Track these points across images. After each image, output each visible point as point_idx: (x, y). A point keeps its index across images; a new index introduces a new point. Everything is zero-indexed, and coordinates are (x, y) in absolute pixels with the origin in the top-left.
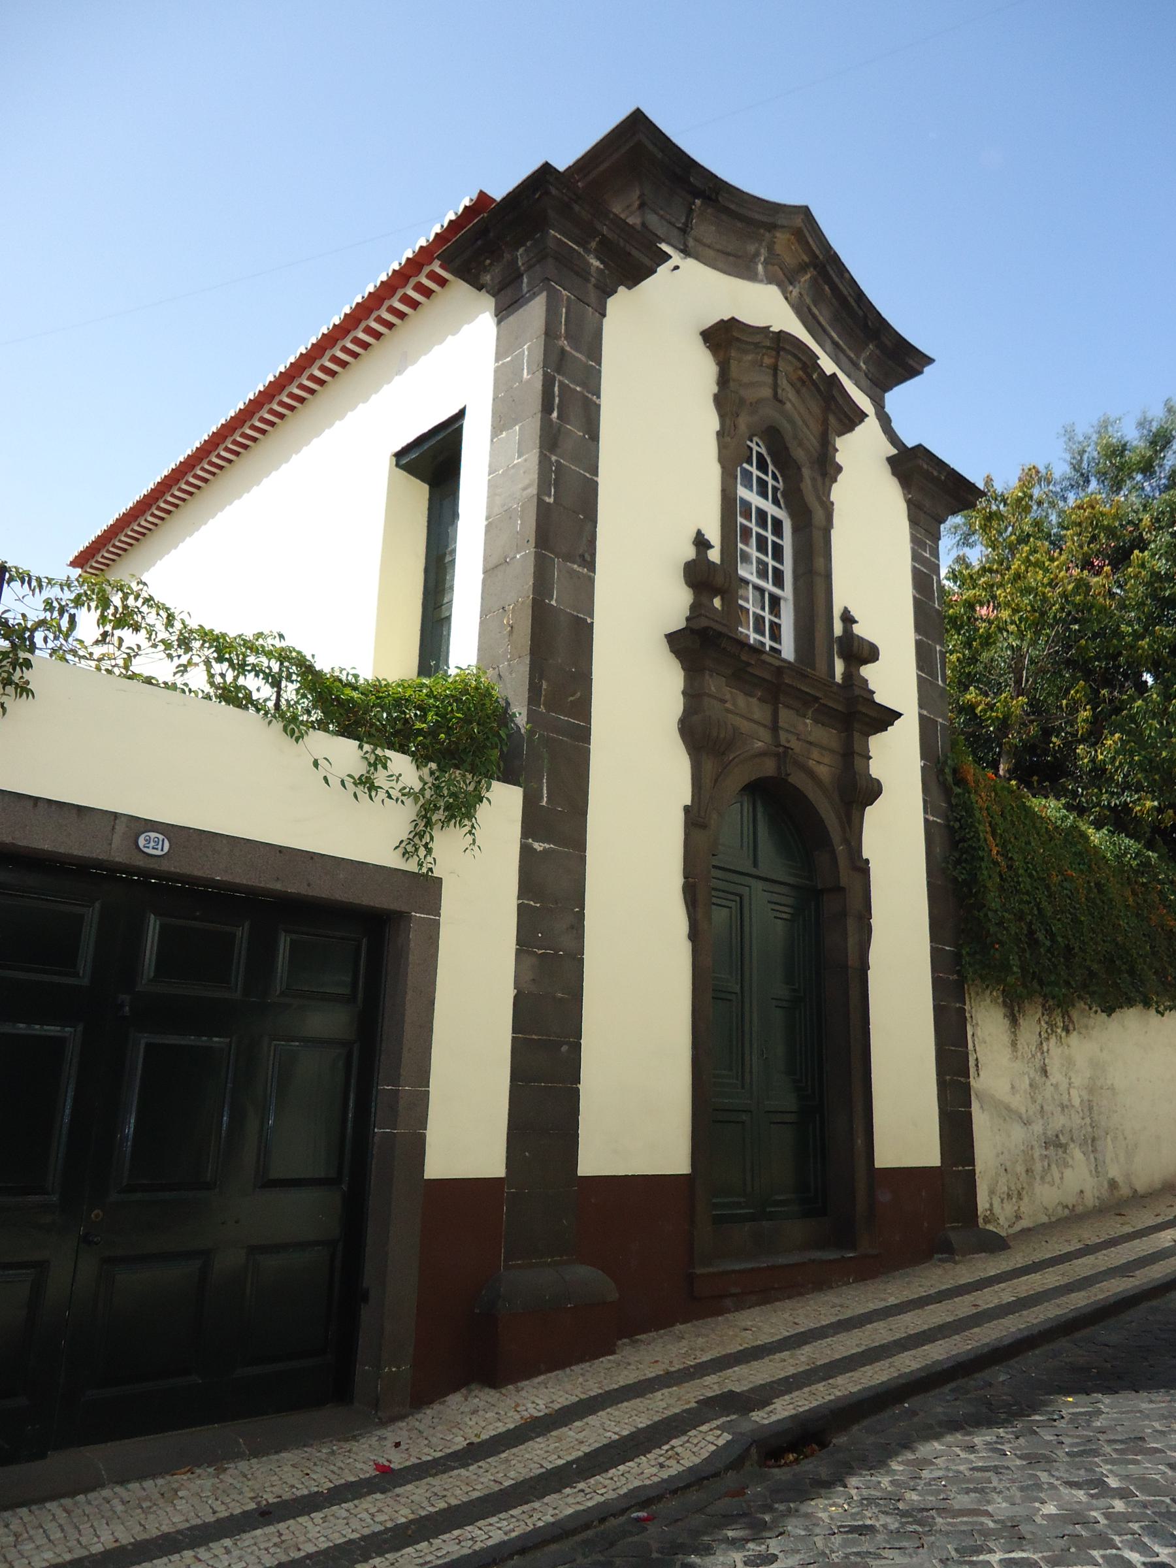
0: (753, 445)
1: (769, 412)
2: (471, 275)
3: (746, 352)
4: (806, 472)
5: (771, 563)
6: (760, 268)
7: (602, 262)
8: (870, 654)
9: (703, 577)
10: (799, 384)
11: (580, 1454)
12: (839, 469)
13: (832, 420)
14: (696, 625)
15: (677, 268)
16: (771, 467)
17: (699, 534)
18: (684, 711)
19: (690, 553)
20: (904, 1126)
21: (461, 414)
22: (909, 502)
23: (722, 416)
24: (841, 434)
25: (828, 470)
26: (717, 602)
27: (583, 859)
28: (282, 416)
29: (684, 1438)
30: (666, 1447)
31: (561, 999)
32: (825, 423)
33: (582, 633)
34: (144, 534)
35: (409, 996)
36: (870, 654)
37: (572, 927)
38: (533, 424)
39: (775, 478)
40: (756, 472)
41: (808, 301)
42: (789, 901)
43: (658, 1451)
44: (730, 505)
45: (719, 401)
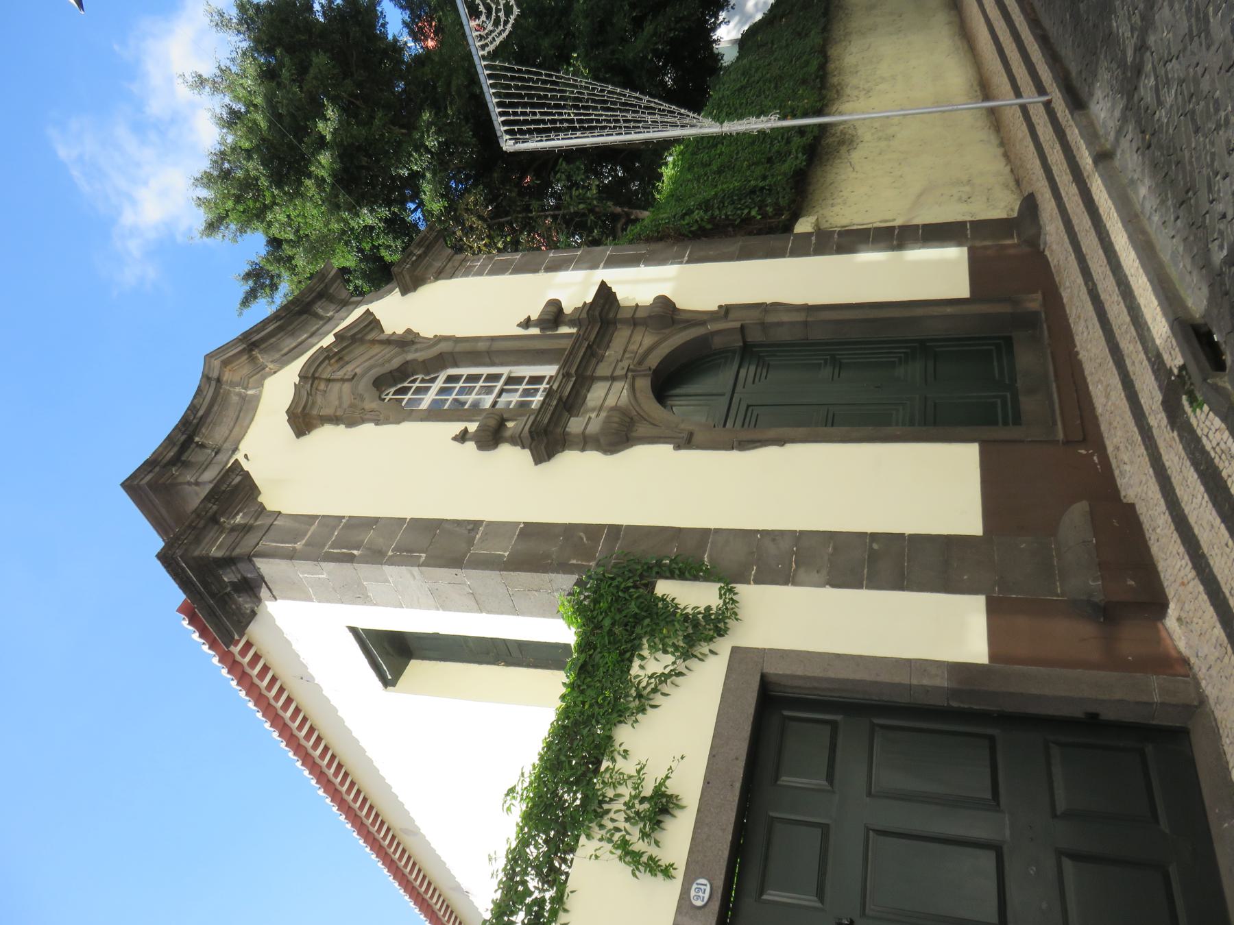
0: (388, 398)
1: (364, 384)
2: (244, 620)
3: (314, 403)
4: (410, 357)
5: (481, 383)
6: (250, 392)
7: (237, 514)
8: (555, 305)
9: (492, 435)
10: (341, 363)
11: (1223, 526)
12: (409, 331)
13: (370, 337)
14: (527, 441)
15: (246, 457)
16: (406, 384)
17: (455, 439)
18: (597, 450)
19: (471, 446)
20: (937, 274)
21: (354, 631)
22: (437, 278)
23: (363, 421)
24: (383, 331)
25: (408, 340)
26: (510, 424)
27: (717, 531)
28: (352, 784)
29: (1204, 440)
30: (1213, 454)
31: (835, 549)
32: (373, 342)
33: (532, 531)
34: (448, 907)
35: (831, 674)
36: (555, 305)
37: (774, 540)
38: (364, 570)
39: (414, 381)
40: (409, 396)
41: (277, 356)
42: (752, 368)
43: (1217, 460)
44: (436, 414)
45: (351, 423)
